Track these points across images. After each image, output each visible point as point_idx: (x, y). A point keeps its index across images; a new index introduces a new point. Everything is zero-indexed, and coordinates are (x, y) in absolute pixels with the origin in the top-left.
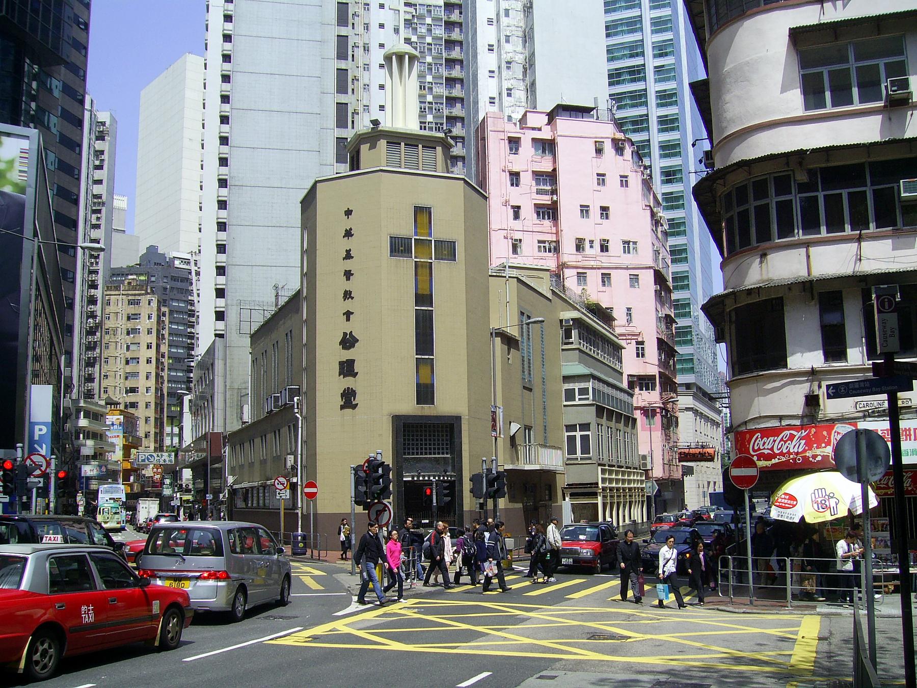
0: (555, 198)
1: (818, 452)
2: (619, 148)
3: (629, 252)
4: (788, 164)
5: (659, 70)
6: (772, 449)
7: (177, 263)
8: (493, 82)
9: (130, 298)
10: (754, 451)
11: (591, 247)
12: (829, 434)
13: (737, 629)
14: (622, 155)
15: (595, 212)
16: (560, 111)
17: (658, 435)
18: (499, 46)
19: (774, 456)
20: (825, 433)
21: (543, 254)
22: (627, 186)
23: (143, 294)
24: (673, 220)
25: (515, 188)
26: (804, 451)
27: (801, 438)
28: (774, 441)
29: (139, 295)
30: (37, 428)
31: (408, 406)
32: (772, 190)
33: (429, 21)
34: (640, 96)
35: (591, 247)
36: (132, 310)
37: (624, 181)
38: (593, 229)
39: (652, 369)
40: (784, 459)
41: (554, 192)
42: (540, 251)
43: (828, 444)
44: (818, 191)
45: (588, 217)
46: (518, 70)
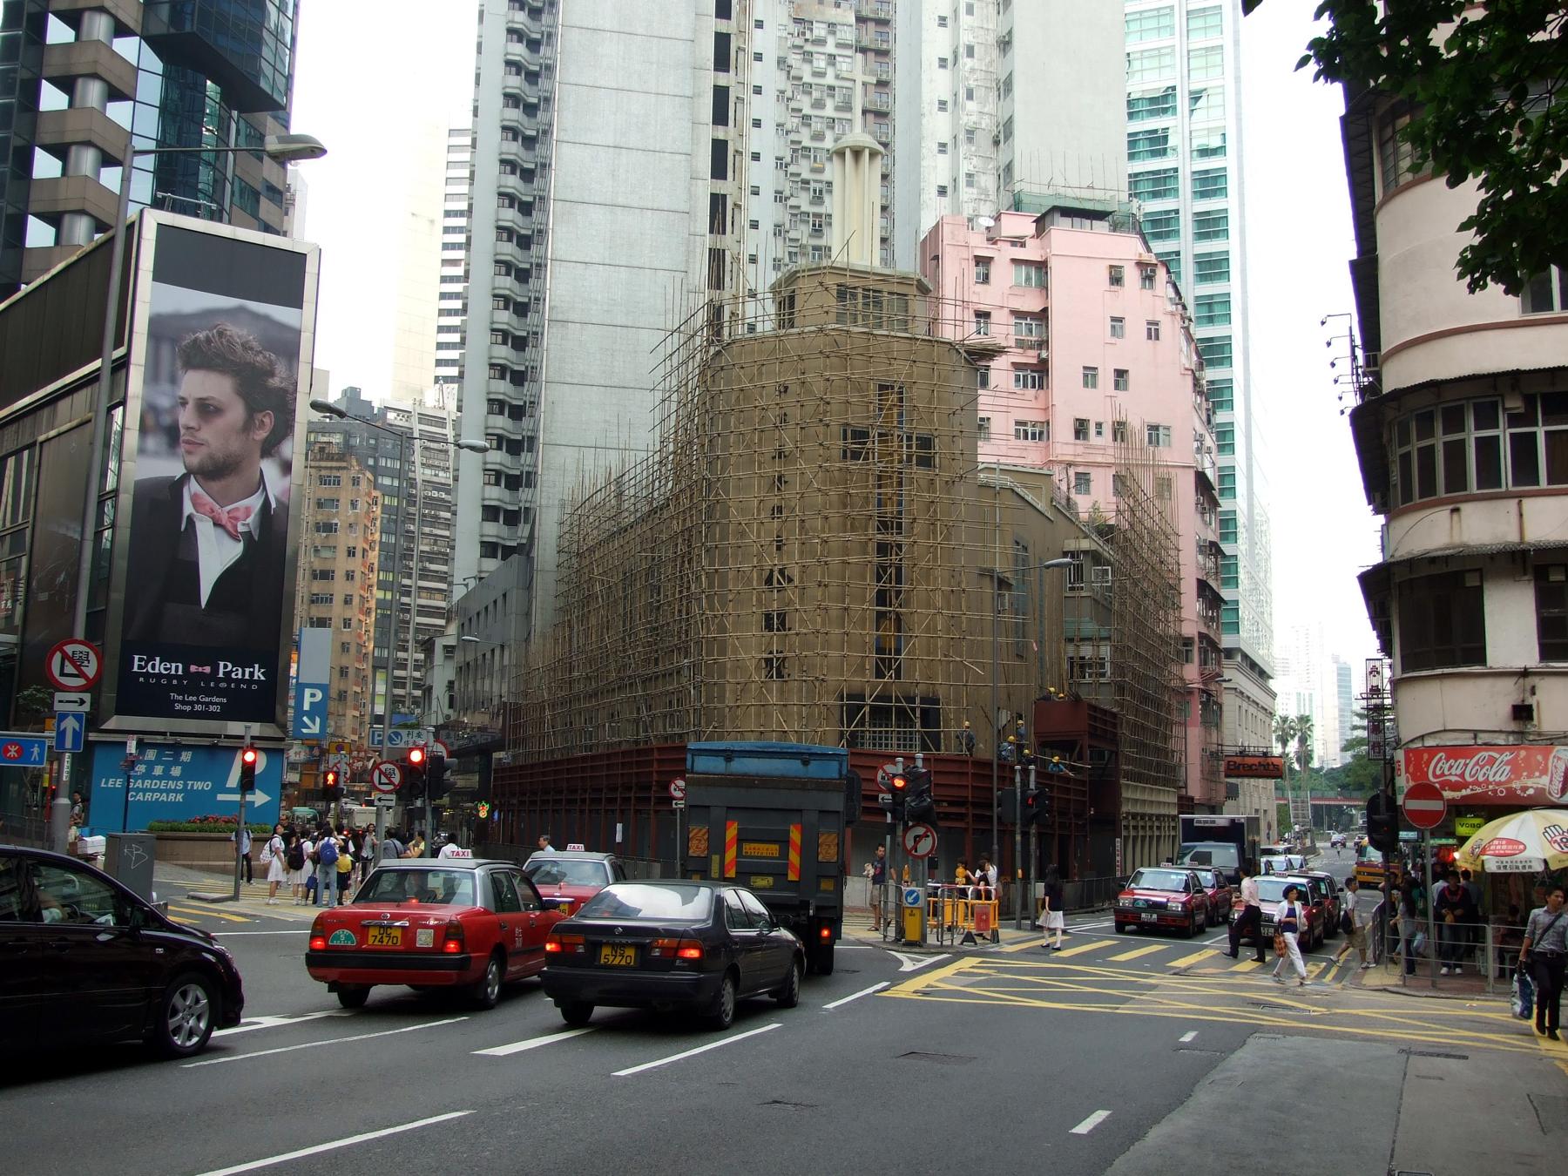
0: (1044, 355)
1: (1529, 783)
2: (1147, 273)
4: (1495, 388)
6: (1462, 775)
7: (391, 416)
8: (943, 161)
9: (323, 473)
10: (1435, 776)
11: (1099, 433)
12: (1546, 759)
13: (1395, 1015)
15: (1106, 378)
16: (1057, 217)
18: (955, 103)
19: (1465, 785)
20: (1540, 758)
21: (1022, 442)
22: (1157, 338)
25: (1090, 390)
26: (1509, 781)
27: (1508, 763)
28: (1466, 765)
29: (339, 468)
30: (308, 692)
31: (867, 682)
32: (1471, 422)
33: (830, 48)
35: (1099, 433)
36: (325, 492)
37: (1153, 332)
38: (1098, 405)
40: (1479, 790)
41: (1044, 344)
42: (1017, 437)
43: (1544, 772)
44: (1536, 425)
45: (1094, 386)
46: (983, 140)
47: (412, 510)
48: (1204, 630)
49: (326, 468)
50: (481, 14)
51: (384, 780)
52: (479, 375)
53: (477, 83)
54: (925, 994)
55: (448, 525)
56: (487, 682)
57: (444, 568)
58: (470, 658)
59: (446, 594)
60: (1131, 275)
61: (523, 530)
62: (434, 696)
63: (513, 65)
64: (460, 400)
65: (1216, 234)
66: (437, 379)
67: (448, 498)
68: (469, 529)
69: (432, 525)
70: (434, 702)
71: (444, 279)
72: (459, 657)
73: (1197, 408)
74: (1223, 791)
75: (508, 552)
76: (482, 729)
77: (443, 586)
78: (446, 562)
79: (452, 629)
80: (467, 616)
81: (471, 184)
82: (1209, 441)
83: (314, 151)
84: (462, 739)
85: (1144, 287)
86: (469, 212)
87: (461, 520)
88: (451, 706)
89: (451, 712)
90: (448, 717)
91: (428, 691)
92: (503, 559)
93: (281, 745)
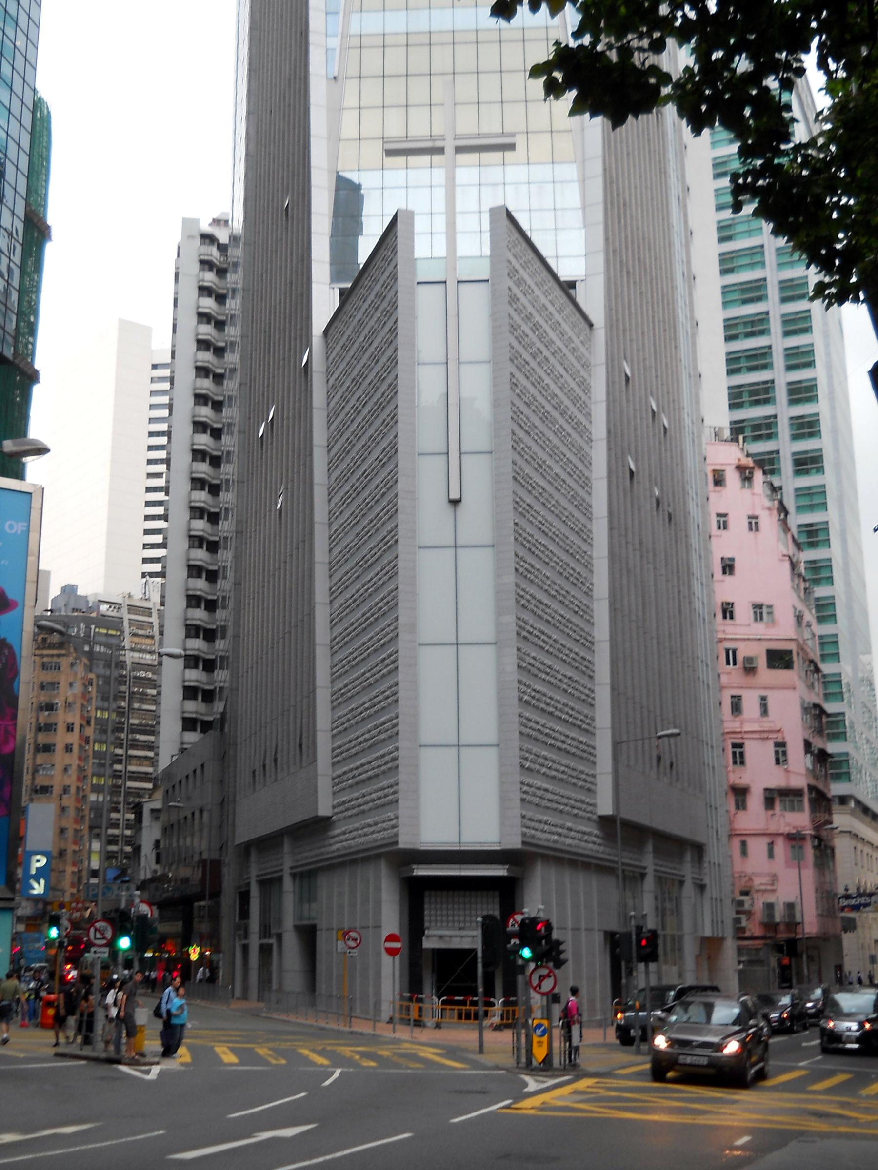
2: (745, 474)
3: (761, 619)
5: (787, 320)
9: (45, 659)
14: (751, 486)
17: (809, 874)
22: (757, 530)
23: (63, 655)
24: (814, 562)
29: (59, 656)
34: (761, 321)
37: (754, 524)
39: (799, 781)
47: (123, 688)
48: (813, 782)
49: (47, 656)
50: (177, 275)
51: (98, 935)
52: (178, 573)
53: (174, 331)
54: (542, 1109)
55: (157, 703)
56: (189, 840)
57: (152, 738)
58: (174, 818)
59: (153, 762)
60: (732, 478)
61: (219, 707)
62: (143, 853)
63: (204, 317)
64: (163, 597)
65: (811, 435)
66: (144, 575)
67: (155, 677)
68: (171, 706)
69: (141, 701)
70: (143, 859)
71: (149, 490)
72: (163, 817)
73: (796, 589)
74: (839, 924)
75: (206, 726)
76: (185, 881)
77: (151, 754)
78: (152, 733)
79: (159, 795)
80: (170, 783)
81: (172, 384)
82: (809, 616)
83: (41, 450)
84: (169, 890)
85: (743, 487)
86: (167, 461)
87: (165, 699)
88: (158, 861)
89: (158, 867)
90: (155, 871)
91: (137, 849)
92: (202, 731)
93: (12, 905)
